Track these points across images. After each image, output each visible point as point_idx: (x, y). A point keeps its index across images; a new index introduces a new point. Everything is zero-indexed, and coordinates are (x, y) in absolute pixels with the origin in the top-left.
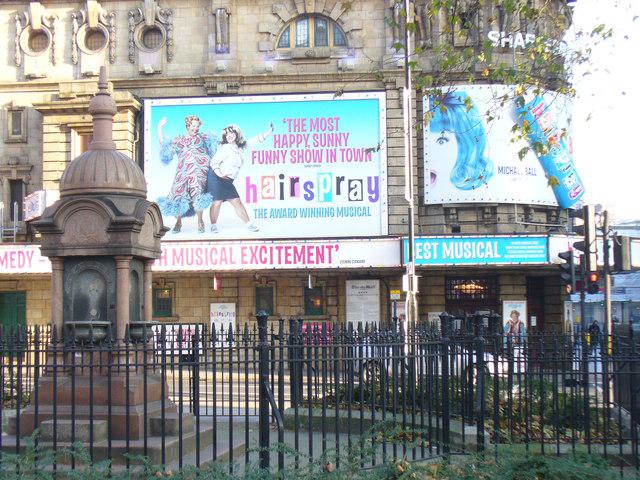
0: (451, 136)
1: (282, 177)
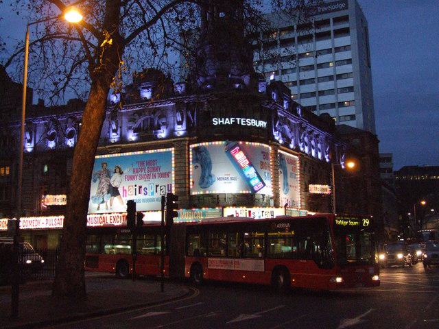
0: (199, 165)
1: (136, 186)
